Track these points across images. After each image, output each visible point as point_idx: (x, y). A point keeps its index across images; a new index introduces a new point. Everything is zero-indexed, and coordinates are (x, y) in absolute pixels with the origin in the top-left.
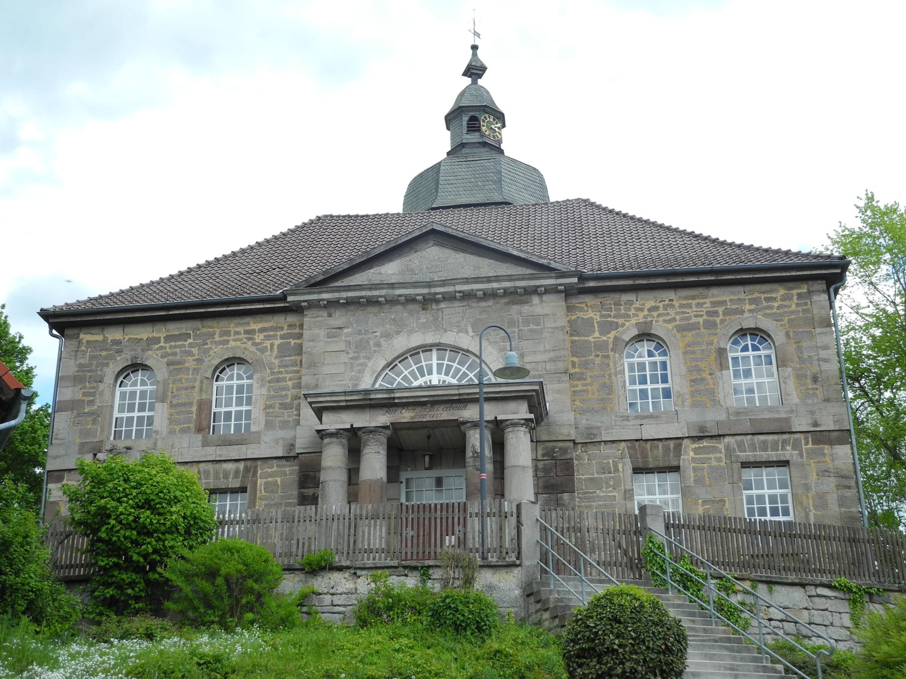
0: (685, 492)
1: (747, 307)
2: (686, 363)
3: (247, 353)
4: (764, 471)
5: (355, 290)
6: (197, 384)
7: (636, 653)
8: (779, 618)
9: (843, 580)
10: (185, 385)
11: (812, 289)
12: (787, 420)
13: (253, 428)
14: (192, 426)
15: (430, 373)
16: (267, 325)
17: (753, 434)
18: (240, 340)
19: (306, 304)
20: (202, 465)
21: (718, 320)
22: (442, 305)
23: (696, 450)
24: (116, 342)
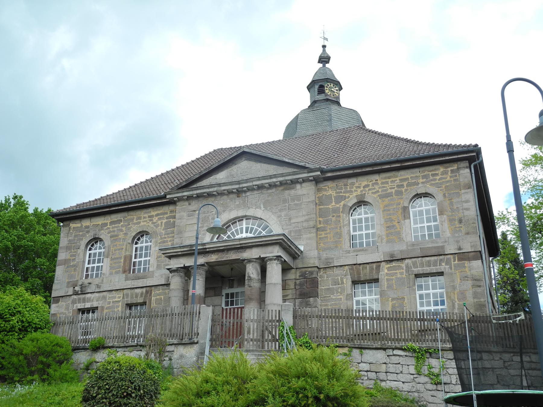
0: (382, 294)
1: (421, 180)
2: (384, 217)
3: (149, 228)
4: (430, 279)
5: (200, 189)
6: (124, 247)
7: (106, 399)
8: (366, 369)
9: (410, 344)
10: (118, 248)
11: (460, 166)
12: (443, 247)
13: (151, 269)
14: (121, 270)
15: (242, 233)
16: (159, 212)
17: (422, 257)
18: (146, 221)
19: (176, 199)
20: (125, 290)
21: (403, 190)
22: (248, 194)
23: (388, 269)
24: (87, 227)
